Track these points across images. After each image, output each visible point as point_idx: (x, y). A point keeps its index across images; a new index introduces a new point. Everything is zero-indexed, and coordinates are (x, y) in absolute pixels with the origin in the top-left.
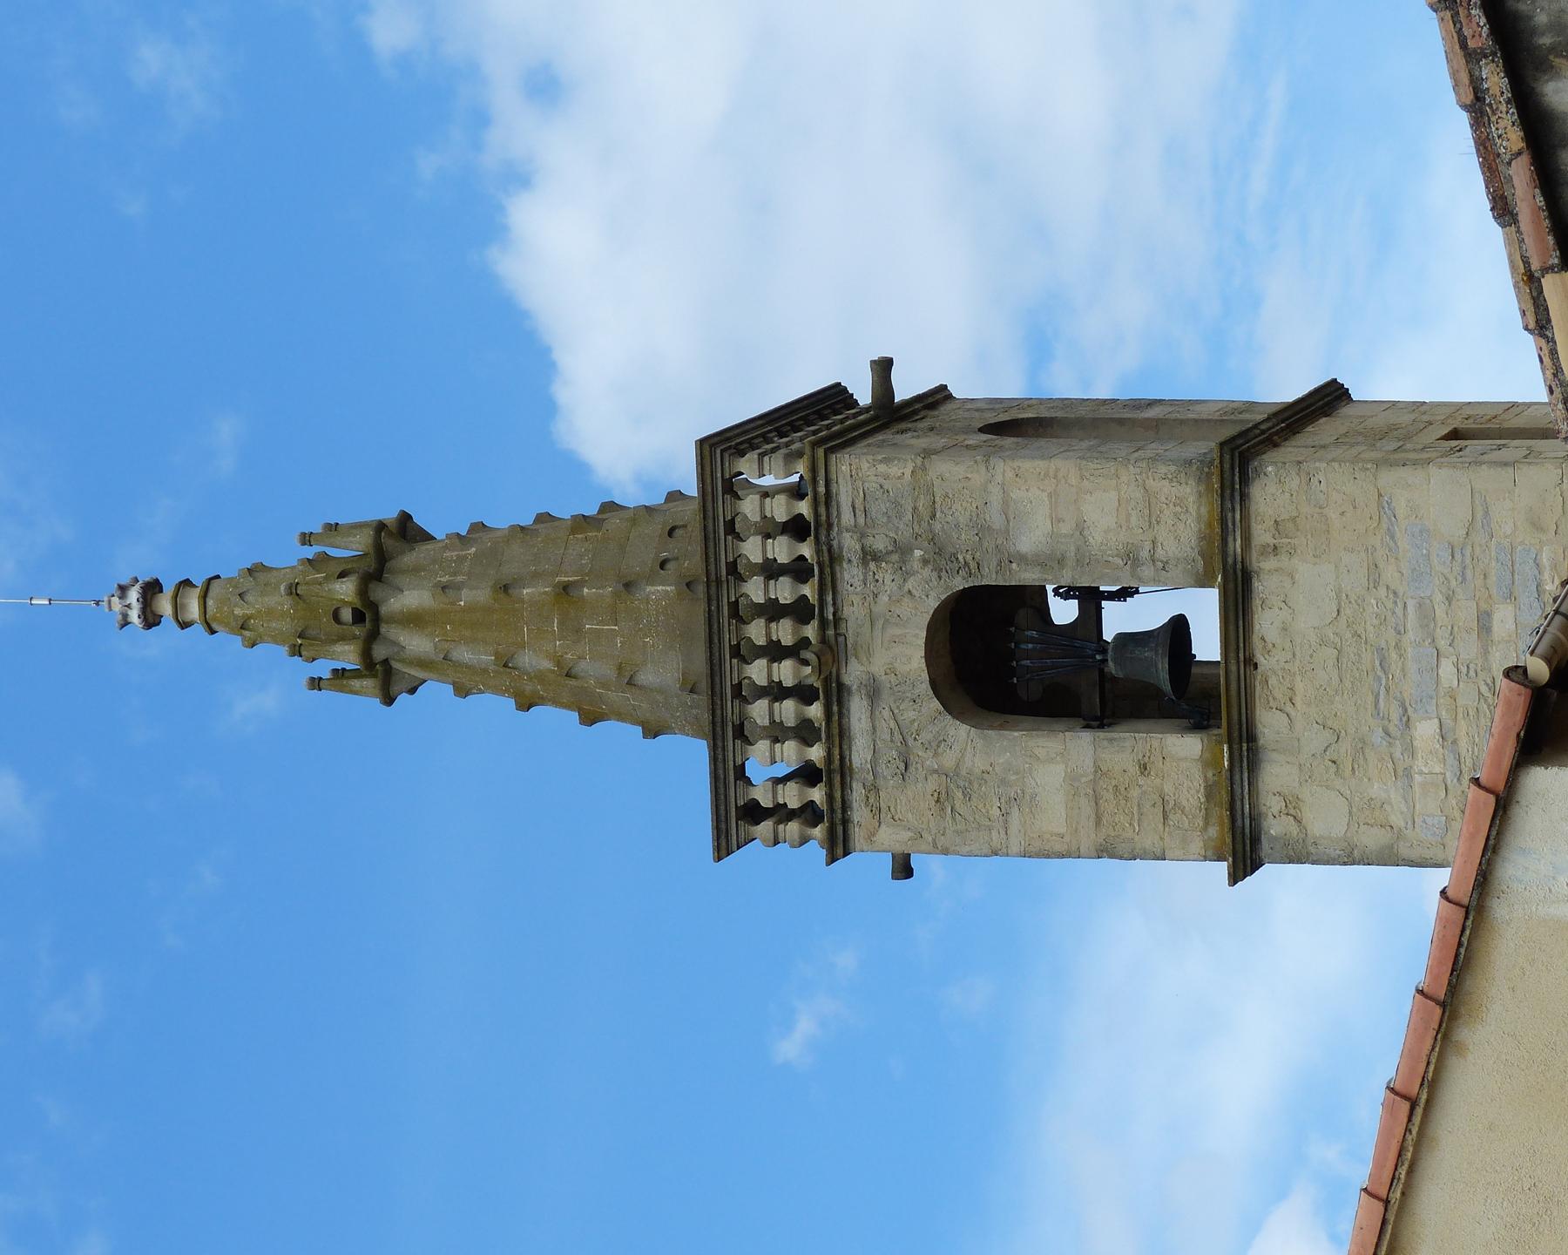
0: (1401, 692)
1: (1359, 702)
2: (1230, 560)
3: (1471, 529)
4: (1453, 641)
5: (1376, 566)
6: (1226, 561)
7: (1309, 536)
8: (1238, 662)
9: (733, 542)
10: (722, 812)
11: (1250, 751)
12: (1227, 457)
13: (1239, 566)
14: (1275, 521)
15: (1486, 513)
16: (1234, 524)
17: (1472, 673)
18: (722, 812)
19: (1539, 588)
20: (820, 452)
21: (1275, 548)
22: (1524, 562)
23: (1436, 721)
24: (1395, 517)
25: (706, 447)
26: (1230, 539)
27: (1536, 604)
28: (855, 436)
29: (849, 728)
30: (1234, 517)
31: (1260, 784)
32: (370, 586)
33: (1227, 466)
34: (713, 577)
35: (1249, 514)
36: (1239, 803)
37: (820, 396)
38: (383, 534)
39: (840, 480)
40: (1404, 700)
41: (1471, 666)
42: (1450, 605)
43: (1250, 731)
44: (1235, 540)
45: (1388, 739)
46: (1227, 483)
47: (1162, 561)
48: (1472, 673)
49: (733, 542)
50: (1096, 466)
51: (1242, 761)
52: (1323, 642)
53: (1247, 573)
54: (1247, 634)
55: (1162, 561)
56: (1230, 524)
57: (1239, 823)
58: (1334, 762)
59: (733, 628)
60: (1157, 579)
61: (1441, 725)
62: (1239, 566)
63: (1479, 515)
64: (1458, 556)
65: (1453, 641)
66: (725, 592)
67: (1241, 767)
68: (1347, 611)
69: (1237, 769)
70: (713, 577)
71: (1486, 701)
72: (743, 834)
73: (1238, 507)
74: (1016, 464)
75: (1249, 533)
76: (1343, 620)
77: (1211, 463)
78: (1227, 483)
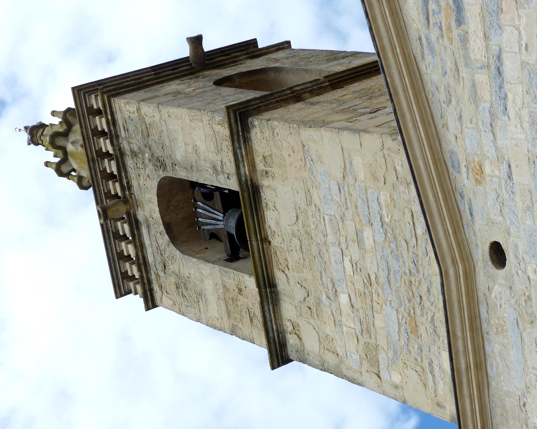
0: (331, 273)
1: (314, 275)
2: (243, 179)
3: (345, 174)
4: (347, 246)
5: (309, 191)
6: (241, 180)
7: (278, 168)
8: (257, 240)
9: (97, 140)
10: (115, 275)
11: (273, 294)
12: (232, 115)
13: (249, 183)
14: (263, 156)
15: (351, 164)
16: (242, 157)
17: (359, 270)
18: (115, 275)
19: (382, 220)
20: (105, 96)
21: (267, 172)
22: (372, 201)
23: (347, 295)
24: (312, 161)
25: (76, 91)
26: (241, 166)
27: (381, 230)
28: (178, 76)
29: (144, 242)
30: (241, 153)
31: (282, 313)
32: (56, 139)
33: (233, 121)
34: (90, 158)
35: (252, 150)
36: (269, 323)
37: (243, 44)
38: (67, 114)
39: (117, 112)
40: (367, 268)
41: (358, 264)
42: (343, 222)
43: (271, 282)
44: (244, 166)
45: (329, 301)
46: (235, 132)
47: (227, 174)
48: (359, 270)
49: (97, 140)
50: (195, 114)
51: (268, 299)
52: (294, 235)
53: (256, 186)
54: (261, 223)
55: (227, 174)
56: (239, 157)
57: (271, 335)
58: (310, 308)
59: (104, 184)
60: (226, 184)
61: (350, 298)
62: (249, 183)
63: (348, 165)
64: (342, 191)
65: (347, 246)
66: (97, 165)
67: (268, 302)
68: (301, 218)
69: (265, 304)
70: (90, 158)
71: (368, 288)
72: (126, 286)
73: (243, 146)
74: (167, 110)
75: (254, 163)
76: (300, 222)
77: (82, 145)
78: (235, 132)
